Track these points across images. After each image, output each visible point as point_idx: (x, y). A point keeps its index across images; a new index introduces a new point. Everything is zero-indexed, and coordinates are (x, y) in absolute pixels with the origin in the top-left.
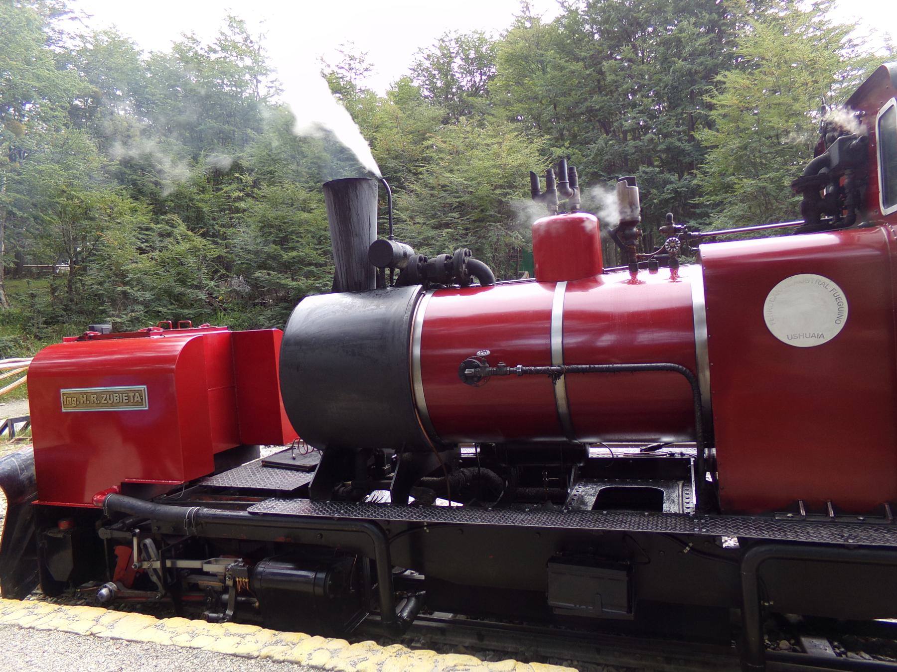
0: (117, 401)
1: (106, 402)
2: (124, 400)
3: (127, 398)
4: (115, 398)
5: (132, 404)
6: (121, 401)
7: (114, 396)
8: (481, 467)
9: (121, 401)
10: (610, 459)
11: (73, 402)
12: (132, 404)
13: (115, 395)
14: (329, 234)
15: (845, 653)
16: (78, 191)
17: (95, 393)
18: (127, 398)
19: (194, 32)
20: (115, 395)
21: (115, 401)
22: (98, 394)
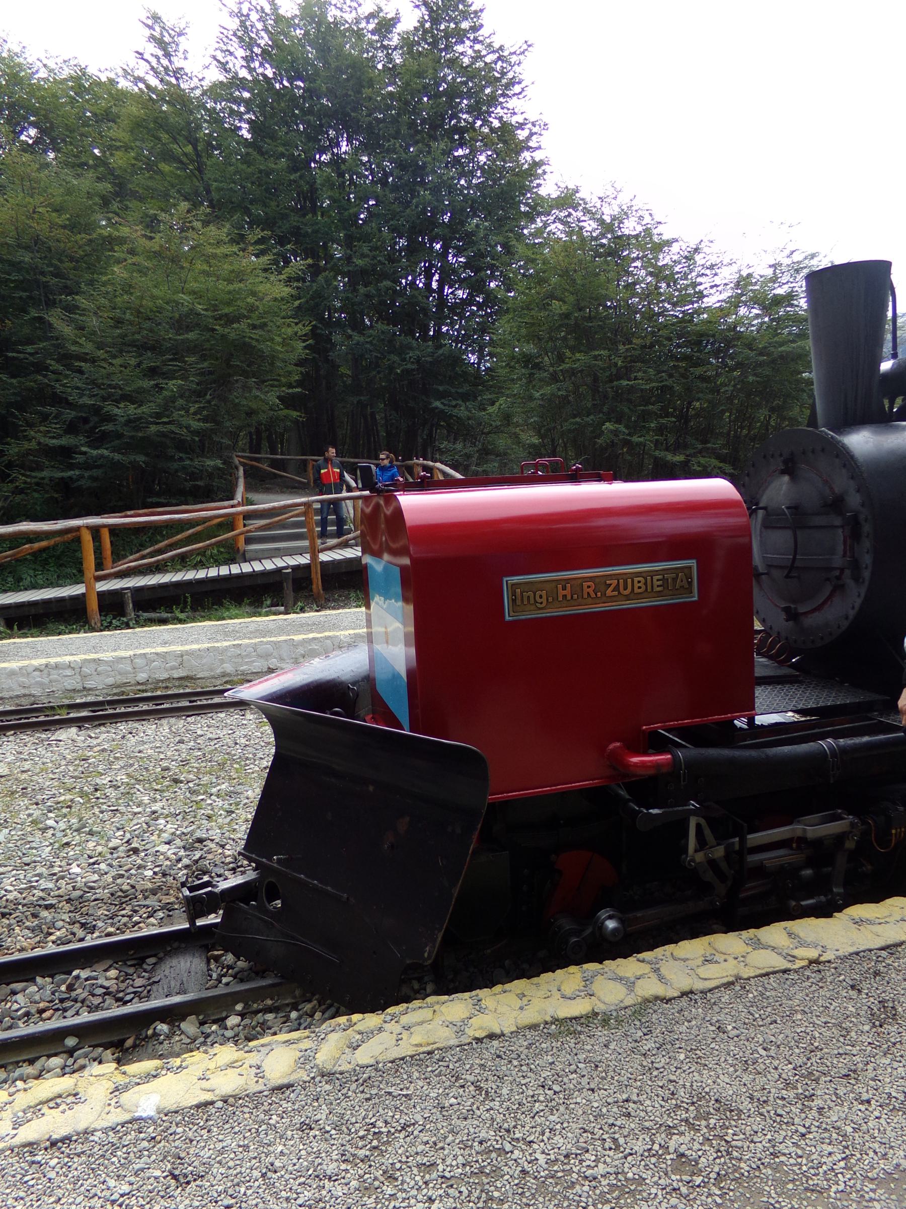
0: (640, 591)
1: (616, 593)
2: (655, 586)
3: (660, 583)
4: (636, 585)
5: (671, 593)
6: (649, 590)
7: (636, 582)
8: (754, 709)
9: (649, 590)
10: (269, 774)
11: (539, 600)
12: (671, 593)
13: (636, 580)
14: (809, 344)
15: (247, 1045)
16: (230, 256)
17: (591, 579)
18: (660, 583)
19: (529, 43)
20: (636, 580)
21: (636, 590)
22: (597, 580)
